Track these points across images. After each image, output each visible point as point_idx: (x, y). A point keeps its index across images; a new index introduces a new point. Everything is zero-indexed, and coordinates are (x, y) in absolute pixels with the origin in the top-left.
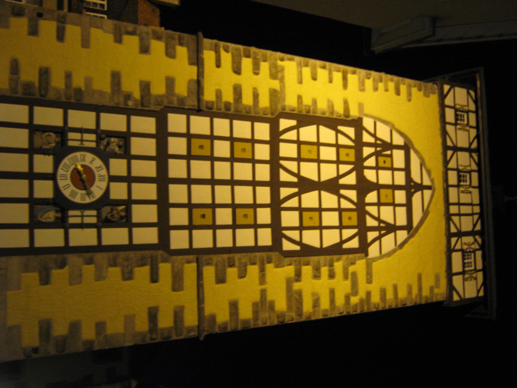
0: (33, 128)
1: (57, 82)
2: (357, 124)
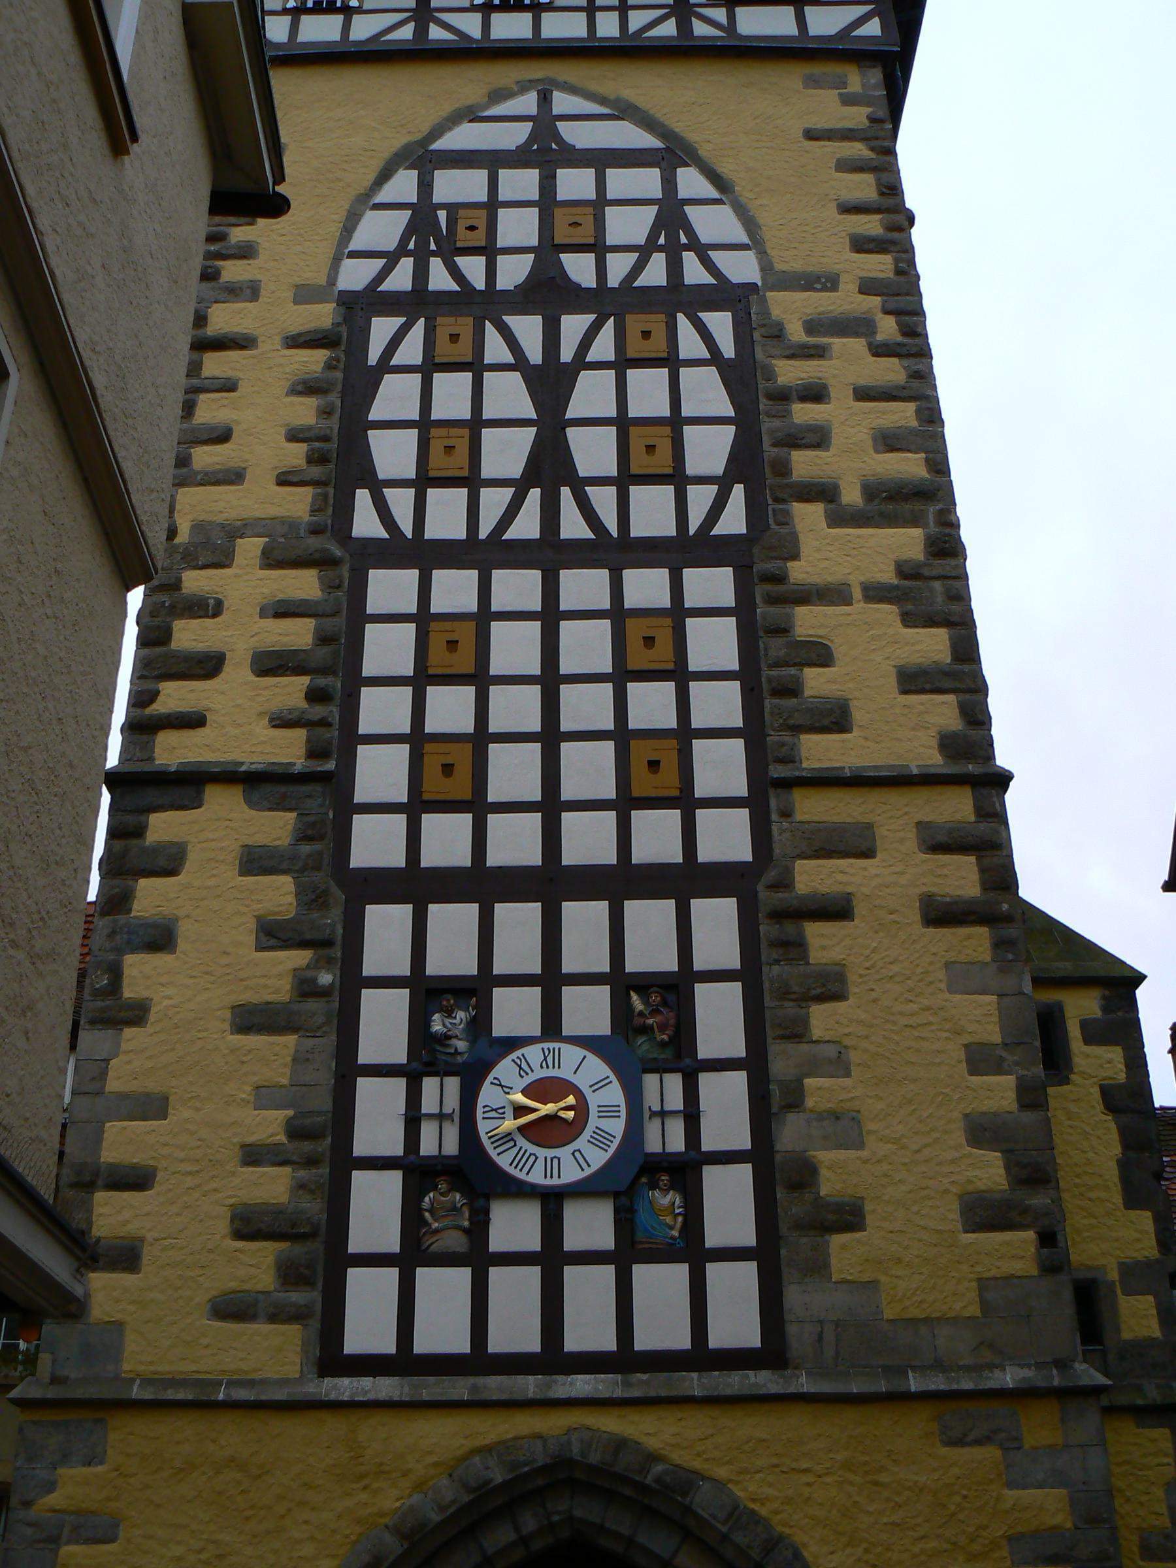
0: (412, 1255)
1: (273, 1186)
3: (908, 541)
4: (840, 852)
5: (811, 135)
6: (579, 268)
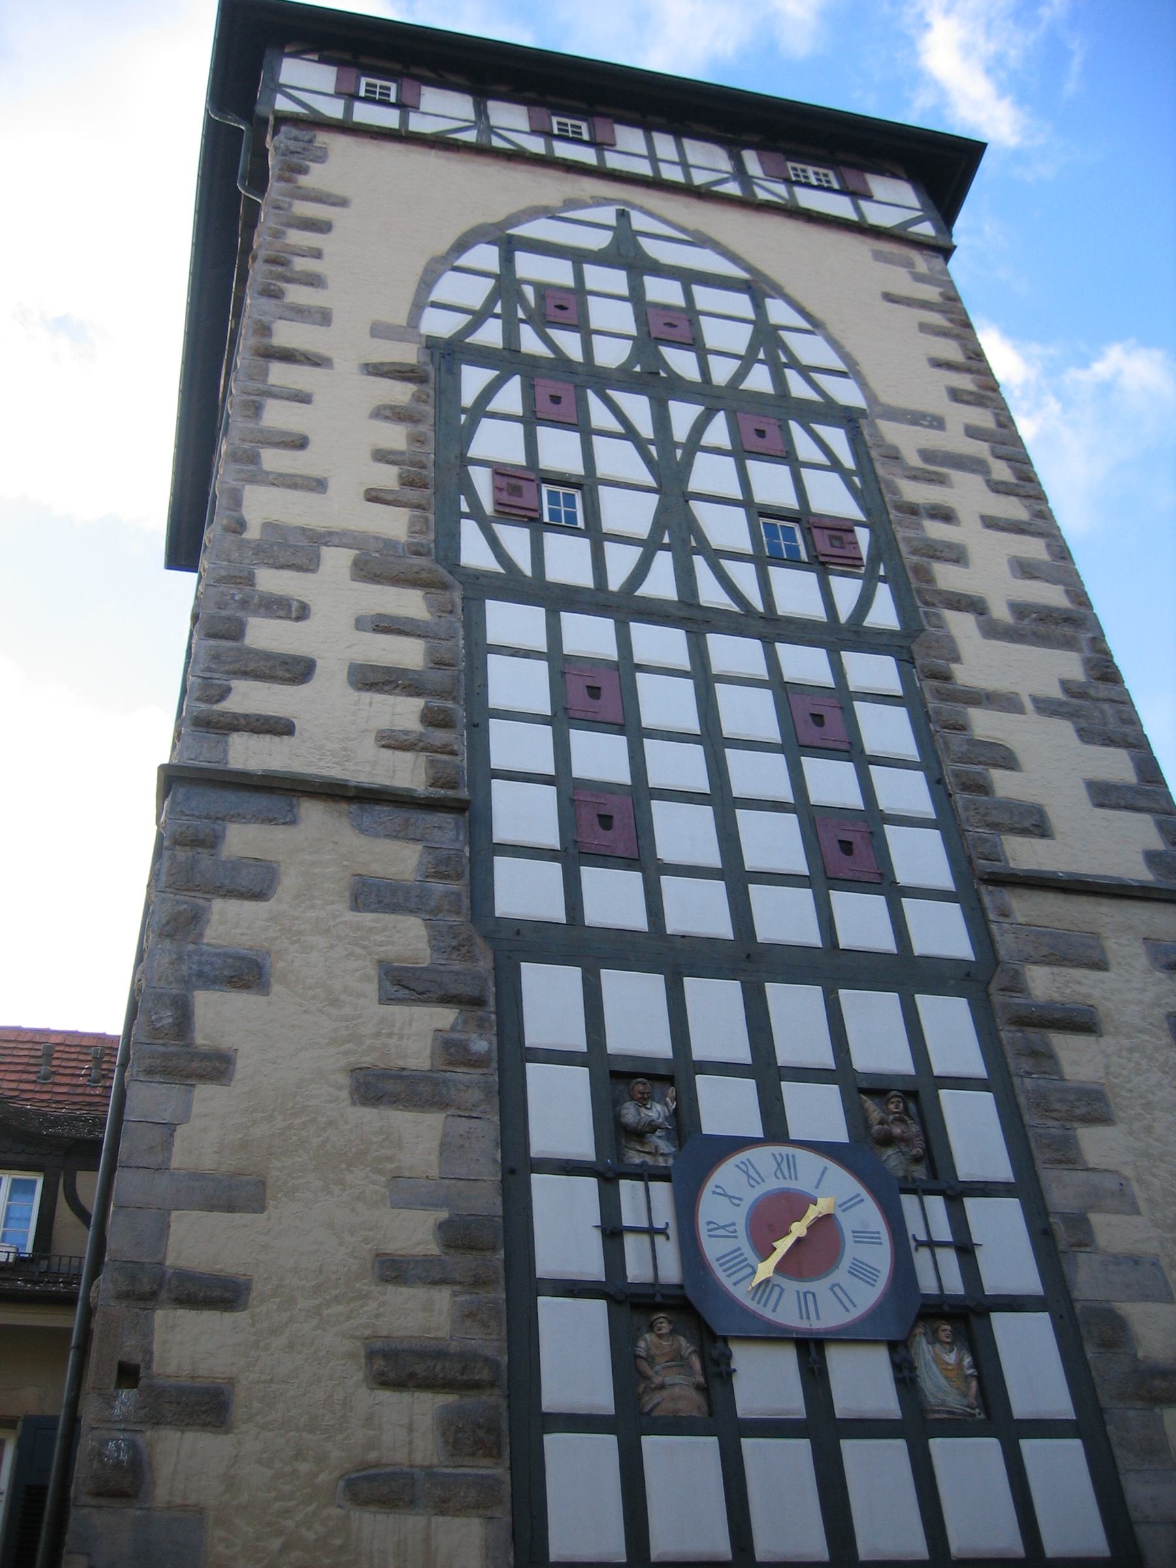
0: (631, 1420)
1: (424, 1314)
2: (450, 354)
3: (1070, 665)
4: (1071, 961)
5: (889, 298)
6: (683, 363)
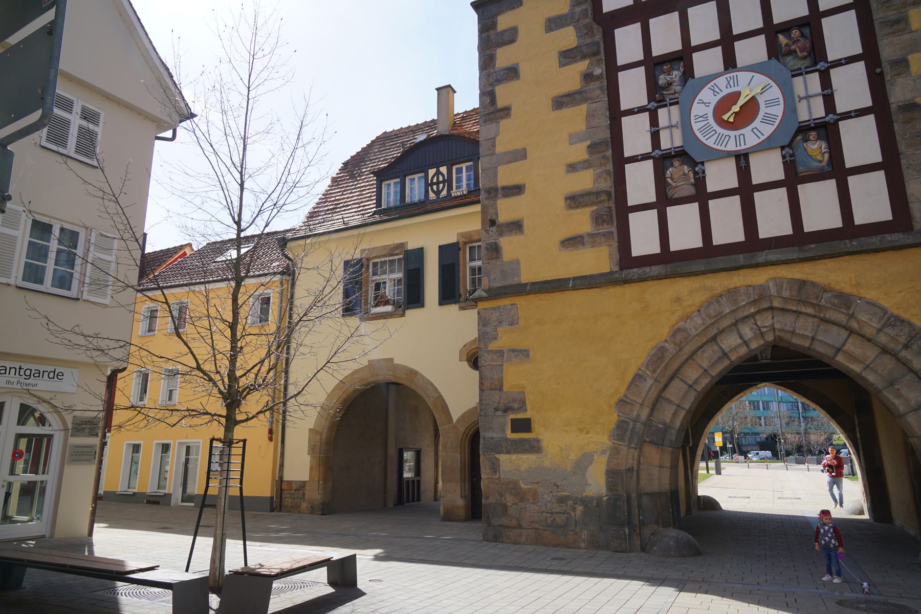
0: (664, 200)
1: (585, 181)
